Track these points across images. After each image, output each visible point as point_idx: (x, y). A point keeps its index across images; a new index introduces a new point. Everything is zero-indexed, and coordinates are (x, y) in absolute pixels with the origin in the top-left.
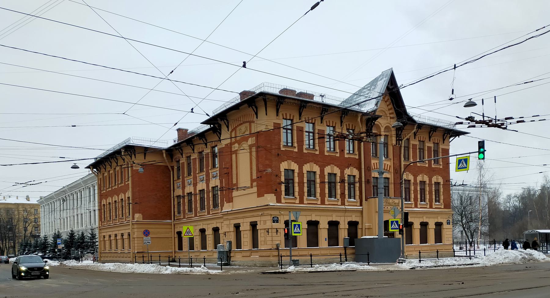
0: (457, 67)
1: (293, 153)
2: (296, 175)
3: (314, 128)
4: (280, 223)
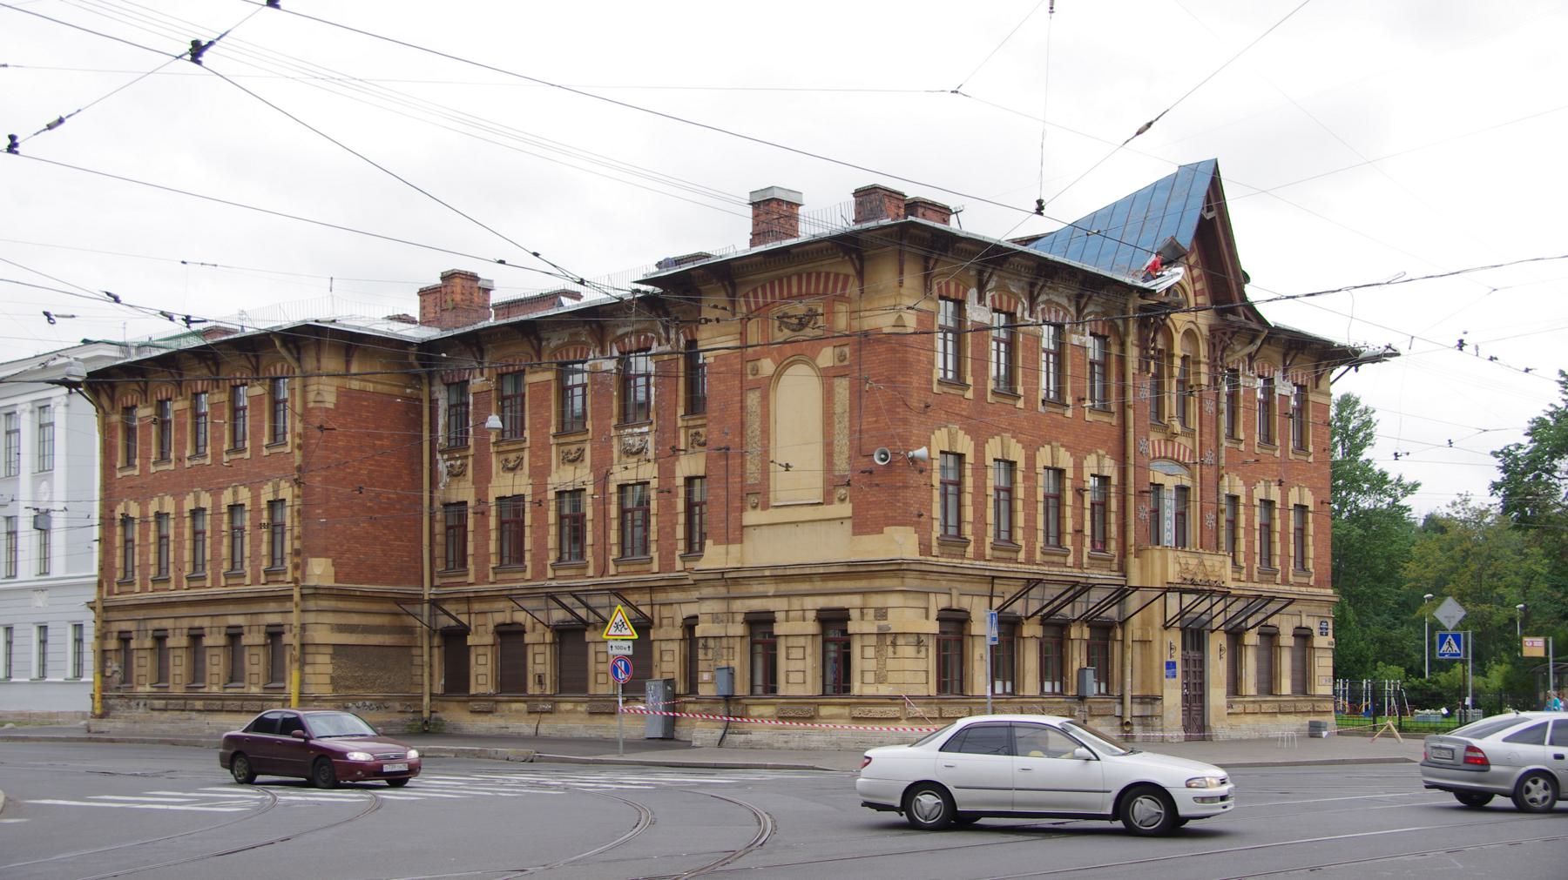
1: (960, 403)
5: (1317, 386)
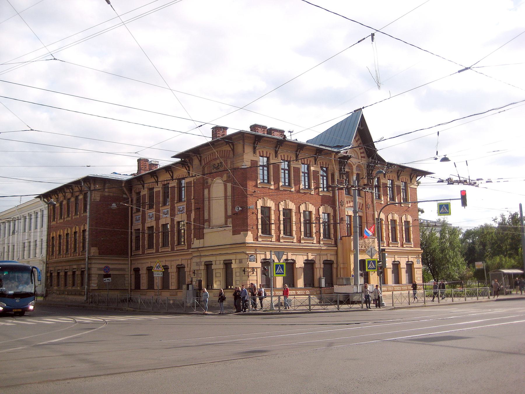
0: (49, 51)
2: (294, 214)
3: (289, 166)
4: (257, 262)
5: (411, 182)
